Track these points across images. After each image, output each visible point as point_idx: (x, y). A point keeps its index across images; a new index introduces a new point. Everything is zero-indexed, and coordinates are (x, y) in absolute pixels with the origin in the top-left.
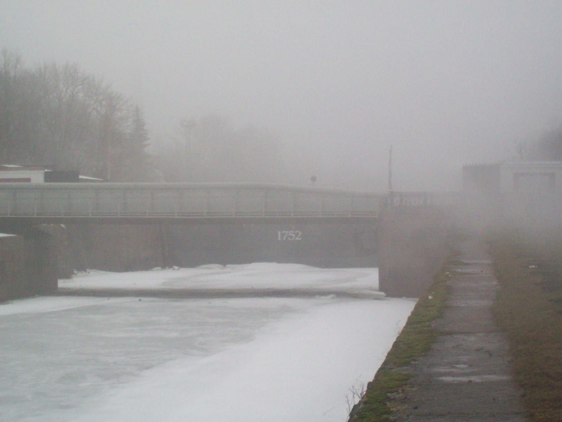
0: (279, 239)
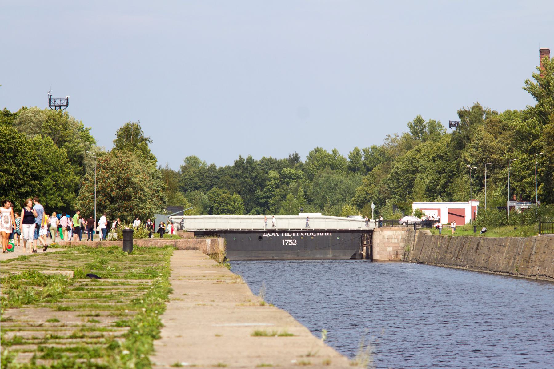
0: (284, 244)
